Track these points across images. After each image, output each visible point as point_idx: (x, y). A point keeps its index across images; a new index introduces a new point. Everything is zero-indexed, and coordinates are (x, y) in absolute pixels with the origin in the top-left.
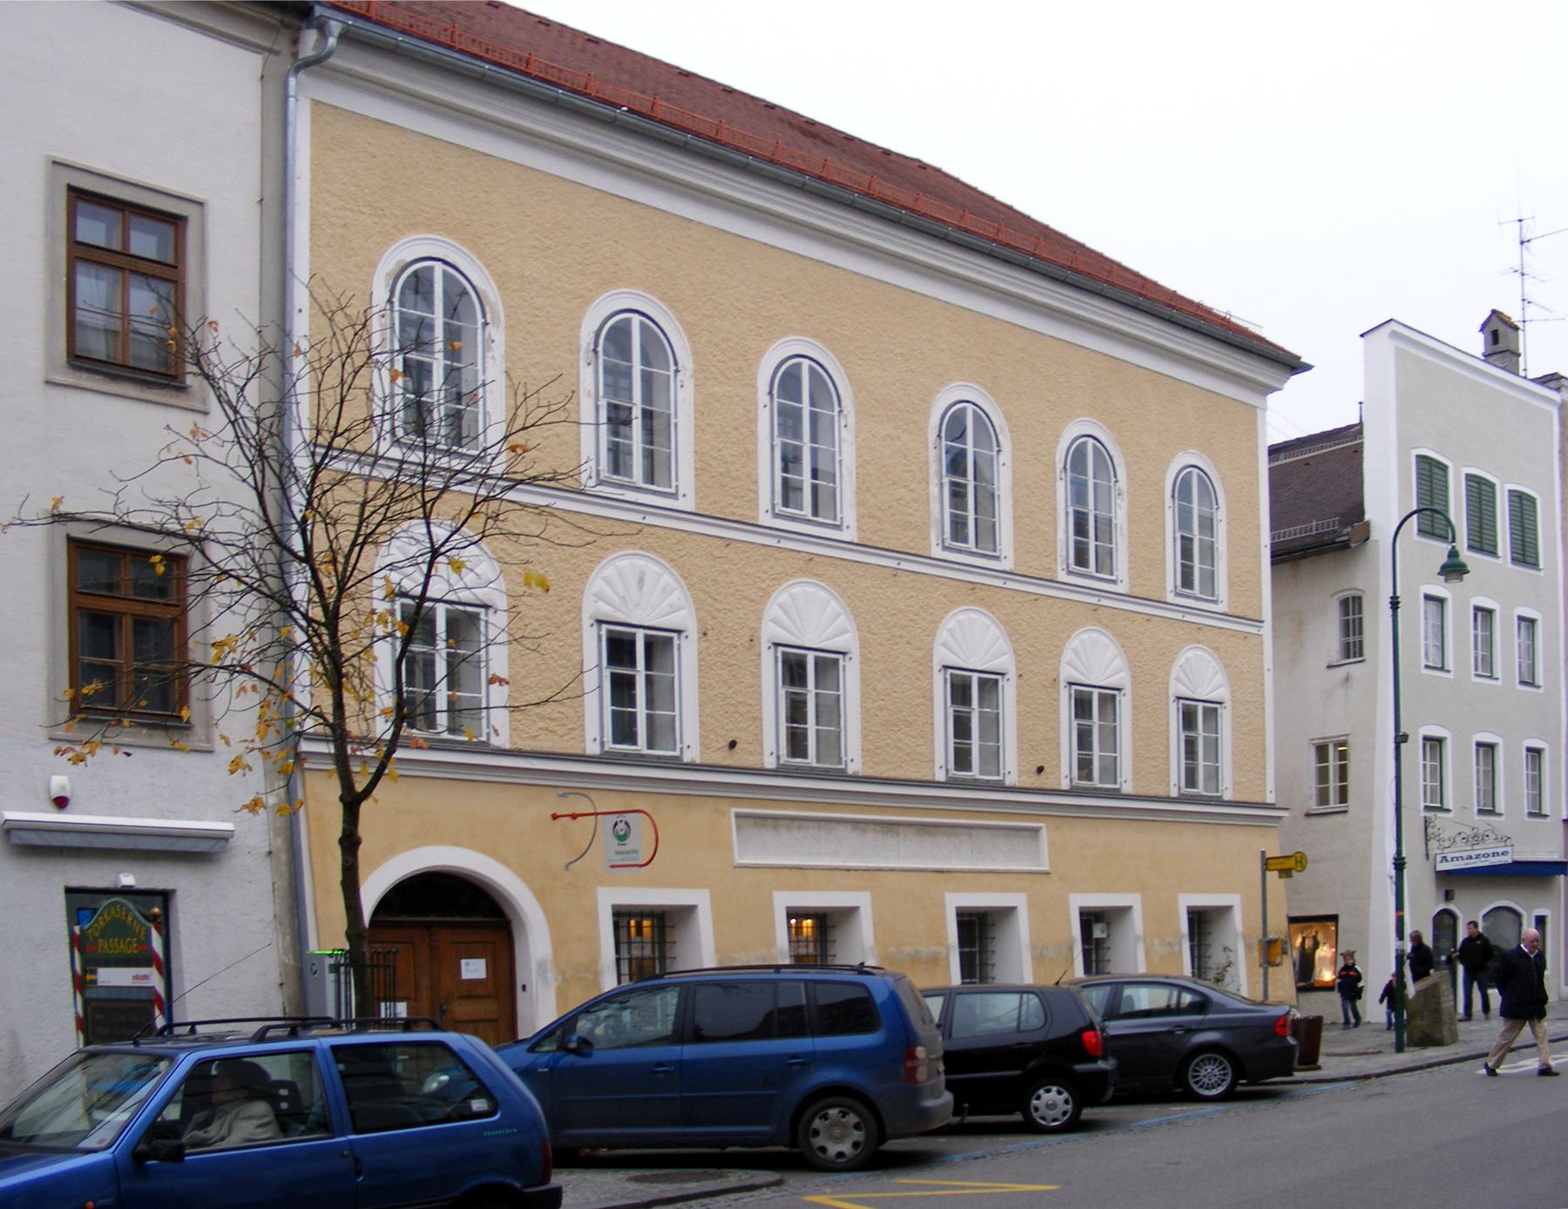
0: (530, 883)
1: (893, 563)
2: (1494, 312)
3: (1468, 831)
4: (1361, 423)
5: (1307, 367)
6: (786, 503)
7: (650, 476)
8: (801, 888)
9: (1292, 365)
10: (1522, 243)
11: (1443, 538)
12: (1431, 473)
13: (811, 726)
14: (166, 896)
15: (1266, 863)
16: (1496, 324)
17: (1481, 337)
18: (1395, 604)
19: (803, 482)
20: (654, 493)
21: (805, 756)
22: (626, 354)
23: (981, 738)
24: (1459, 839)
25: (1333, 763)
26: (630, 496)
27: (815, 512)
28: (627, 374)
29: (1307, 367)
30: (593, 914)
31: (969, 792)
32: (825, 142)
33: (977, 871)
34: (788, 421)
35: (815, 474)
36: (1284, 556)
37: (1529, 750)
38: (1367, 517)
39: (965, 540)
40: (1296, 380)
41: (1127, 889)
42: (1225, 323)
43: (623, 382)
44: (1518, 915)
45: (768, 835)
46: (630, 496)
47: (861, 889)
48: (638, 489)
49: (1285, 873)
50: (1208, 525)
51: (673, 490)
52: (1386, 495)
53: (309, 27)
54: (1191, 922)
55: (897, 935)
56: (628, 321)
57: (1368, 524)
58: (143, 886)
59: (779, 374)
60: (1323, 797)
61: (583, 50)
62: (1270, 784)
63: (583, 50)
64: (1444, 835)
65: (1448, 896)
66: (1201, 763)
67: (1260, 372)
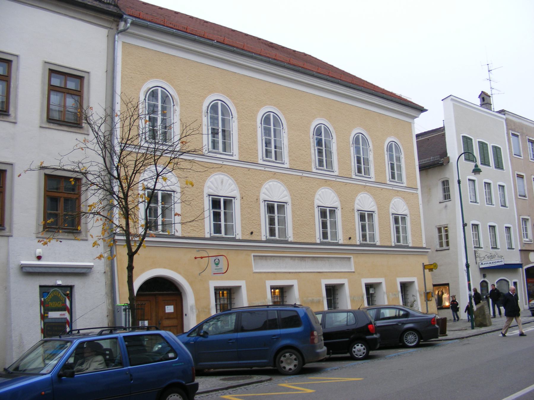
3: (489, 255)
5: (426, 110)
6: (267, 157)
7: (225, 150)
8: (275, 279)
12: (467, 141)
13: (277, 226)
15: (425, 267)
16: (483, 96)
17: (479, 100)
18: (459, 182)
19: (272, 150)
20: (226, 155)
21: (221, 233)
24: (486, 257)
27: (276, 159)
29: (426, 110)
30: (208, 290)
31: (327, 246)
34: (267, 131)
35: (275, 147)
36: (423, 168)
38: (448, 155)
41: (381, 277)
42: (400, 98)
48: (221, 154)
49: (431, 270)
50: (398, 159)
52: (454, 148)
54: (401, 287)
57: (448, 158)
60: (441, 245)
61: (203, 25)
62: (424, 241)
63: (203, 25)
64: (481, 256)
65: (484, 276)
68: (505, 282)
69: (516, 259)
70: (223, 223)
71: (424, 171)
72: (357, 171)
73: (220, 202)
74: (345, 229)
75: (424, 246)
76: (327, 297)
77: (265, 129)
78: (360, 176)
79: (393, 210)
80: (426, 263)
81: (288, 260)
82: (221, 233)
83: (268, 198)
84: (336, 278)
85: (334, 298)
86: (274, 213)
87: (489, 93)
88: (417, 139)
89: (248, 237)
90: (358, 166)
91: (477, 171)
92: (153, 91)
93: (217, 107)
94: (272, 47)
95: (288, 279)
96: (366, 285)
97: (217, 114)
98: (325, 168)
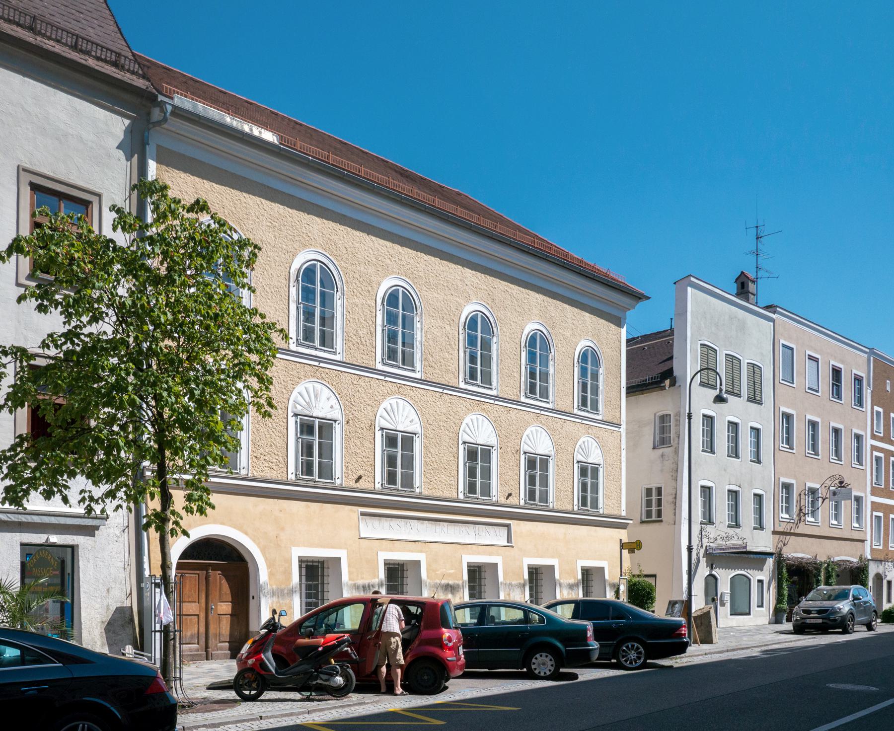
0: (258, 545)
1: (441, 390)
2: (742, 273)
3: (724, 535)
4: (672, 330)
5: (649, 298)
6: (389, 358)
7: (323, 343)
8: (391, 550)
9: (638, 297)
10: (757, 238)
11: (714, 387)
12: (708, 351)
13: (399, 470)
14: (73, 548)
15: (622, 546)
16: (743, 279)
17: (735, 285)
18: (690, 416)
19: (399, 348)
20: (325, 351)
21: (395, 484)
22: (313, 282)
23: (482, 478)
24: (718, 538)
25: (654, 498)
26: (313, 352)
27: (403, 364)
28: (313, 291)
29: (649, 298)
30: (289, 561)
31: (473, 505)
32: (412, 179)
33: (480, 543)
34: (391, 319)
35: (404, 344)
36: (632, 390)
37: (755, 495)
38: (675, 374)
39: (535, 394)
40: (642, 304)
41: (553, 557)
43: (311, 296)
44: (750, 580)
45: (376, 521)
46: (313, 352)
47: (421, 551)
48: (316, 349)
49: (631, 551)
50: (595, 377)
51: (875, 453)
52: (689, 364)
53: (155, 107)
54: (583, 574)
55: (440, 576)
56: (315, 265)
57: (675, 378)
58: (61, 543)
59: (390, 291)
60: (649, 514)
61: (294, 128)
62: (624, 507)
63: (294, 128)
64: (712, 536)
65: (712, 568)
66: (589, 495)
67: (623, 300)
68: (745, 579)
69: (762, 542)
70: (316, 459)
71: (633, 398)
72: (468, 377)
73: (476, 453)
74: (506, 482)
75: (624, 514)
76: (469, 582)
77: (305, 289)
78: (532, 399)
79: (526, 446)
80: (625, 540)
81: (414, 523)
82: (475, 493)
83: (581, 458)
84: (484, 553)
85: (480, 585)
86: (535, 468)
87: (752, 275)
88: (627, 346)
89: (352, 484)
90: (470, 367)
91: (719, 399)
92: (390, 294)
93: (314, 272)
94: (407, 177)
95: (412, 551)
96: (385, 564)
97: (314, 283)
98: (479, 382)
